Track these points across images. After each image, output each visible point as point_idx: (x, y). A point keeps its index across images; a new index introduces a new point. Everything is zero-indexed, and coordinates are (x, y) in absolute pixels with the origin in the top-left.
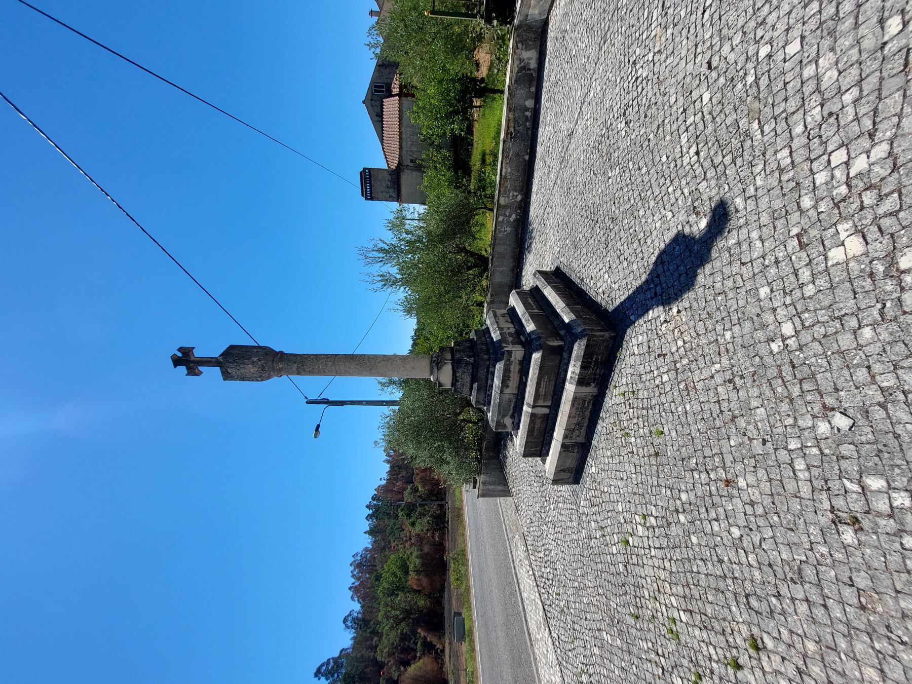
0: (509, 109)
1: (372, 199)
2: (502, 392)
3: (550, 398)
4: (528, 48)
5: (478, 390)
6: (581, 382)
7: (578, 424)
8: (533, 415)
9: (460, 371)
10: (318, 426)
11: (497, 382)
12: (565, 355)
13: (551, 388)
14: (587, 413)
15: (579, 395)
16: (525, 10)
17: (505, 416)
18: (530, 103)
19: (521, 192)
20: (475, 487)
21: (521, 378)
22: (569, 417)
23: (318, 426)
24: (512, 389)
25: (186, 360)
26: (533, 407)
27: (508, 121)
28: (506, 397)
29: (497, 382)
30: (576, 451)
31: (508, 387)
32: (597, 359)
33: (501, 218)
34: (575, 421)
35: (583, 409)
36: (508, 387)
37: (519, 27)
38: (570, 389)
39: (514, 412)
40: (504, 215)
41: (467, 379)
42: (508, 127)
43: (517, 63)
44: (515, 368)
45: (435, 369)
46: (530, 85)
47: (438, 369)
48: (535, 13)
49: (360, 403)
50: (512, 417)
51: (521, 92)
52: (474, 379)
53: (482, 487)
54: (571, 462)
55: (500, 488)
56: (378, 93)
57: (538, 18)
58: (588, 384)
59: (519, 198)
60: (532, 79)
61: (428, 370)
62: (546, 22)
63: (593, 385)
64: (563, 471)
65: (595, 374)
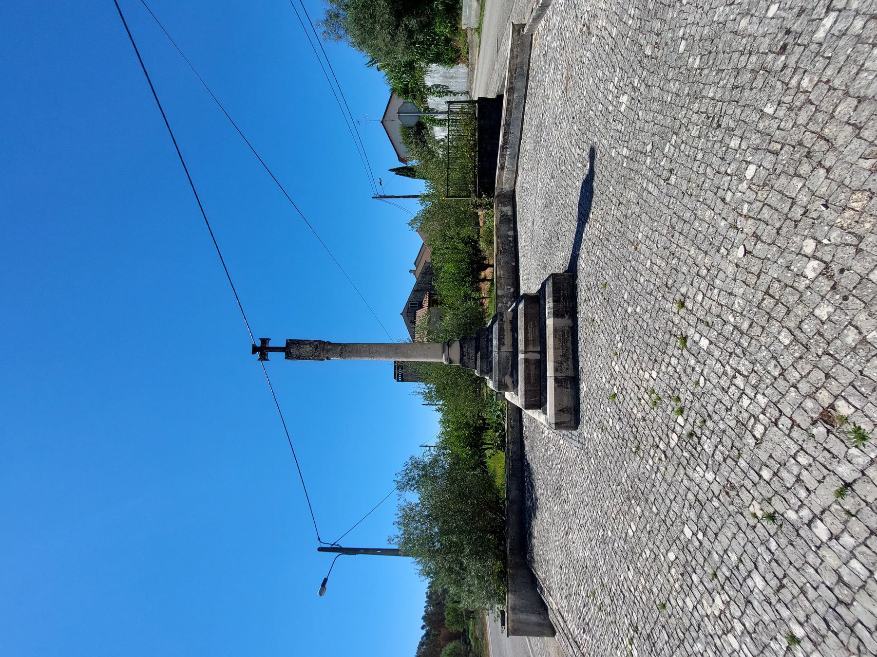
0: (498, 237)
1: (402, 381)
2: (499, 350)
3: (537, 342)
4: (505, 205)
5: (481, 358)
6: (557, 314)
7: (564, 356)
8: (526, 361)
9: (466, 345)
10: (326, 580)
11: (495, 342)
12: (542, 302)
13: (538, 333)
14: (569, 344)
15: (557, 326)
16: (500, 186)
17: (504, 375)
18: (511, 233)
19: (512, 286)
20: (503, 624)
21: (513, 336)
22: (555, 349)
23: (326, 580)
24: (507, 348)
25: (262, 350)
26: (526, 352)
27: (498, 243)
28: (504, 355)
29: (495, 342)
30: (569, 386)
31: (504, 344)
32: (564, 294)
33: (500, 305)
34: (560, 352)
35: (564, 340)
36: (504, 344)
37: (498, 196)
38: (550, 322)
39: (512, 371)
40: (502, 302)
41: (472, 352)
42: (498, 247)
43: (499, 213)
44: (507, 327)
45: (447, 347)
46: (510, 224)
47: (449, 347)
48: (506, 187)
49: (399, 197)
50: (512, 375)
51: (504, 228)
52: (477, 349)
53: (511, 616)
54: (567, 402)
55: (534, 618)
56: (412, 307)
57: (508, 189)
58: (563, 316)
59: (512, 290)
60: (511, 221)
61: (441, 350)
62: (514, 191)
63: (567, 317)
64: (562, 411)
65: (566, 307)
